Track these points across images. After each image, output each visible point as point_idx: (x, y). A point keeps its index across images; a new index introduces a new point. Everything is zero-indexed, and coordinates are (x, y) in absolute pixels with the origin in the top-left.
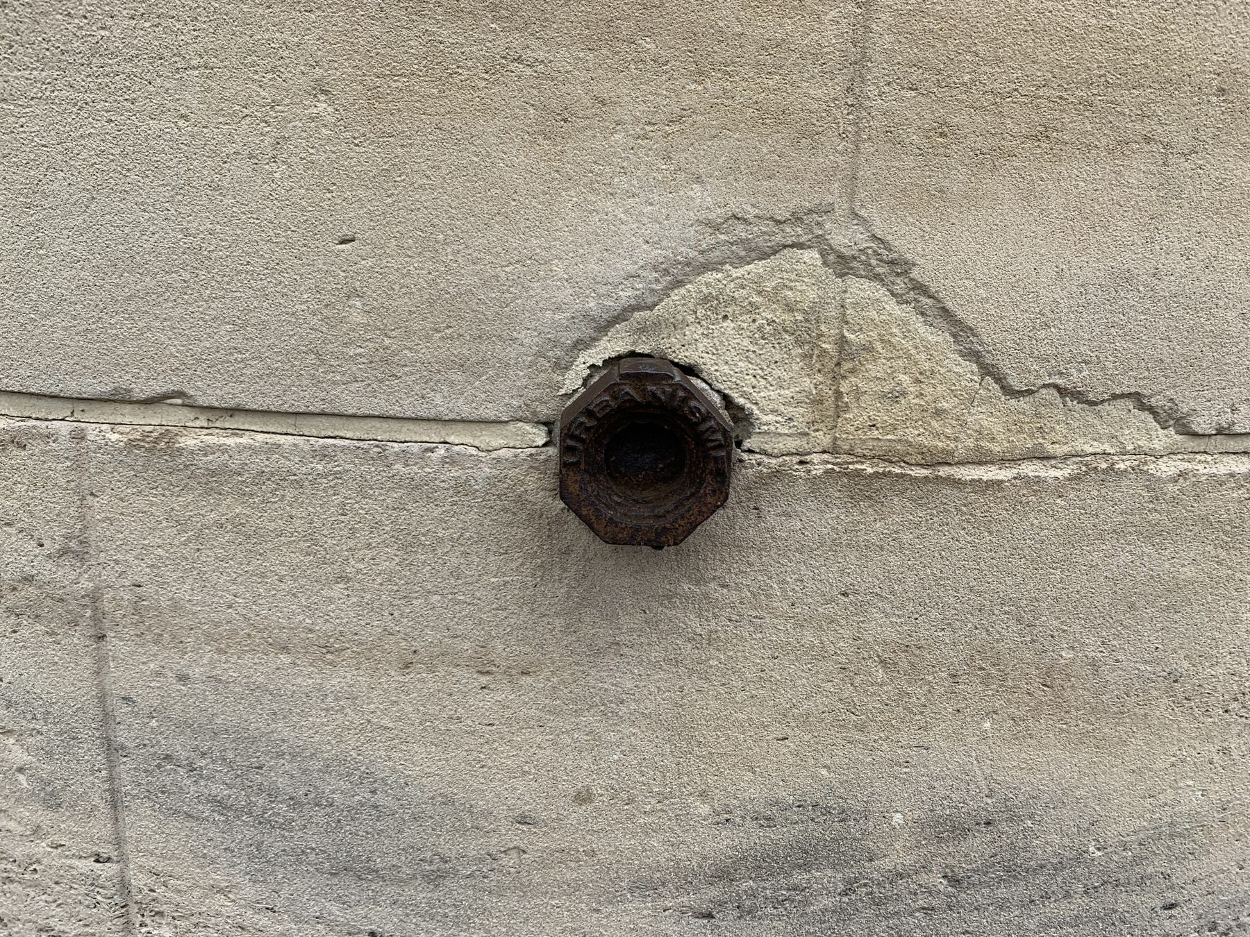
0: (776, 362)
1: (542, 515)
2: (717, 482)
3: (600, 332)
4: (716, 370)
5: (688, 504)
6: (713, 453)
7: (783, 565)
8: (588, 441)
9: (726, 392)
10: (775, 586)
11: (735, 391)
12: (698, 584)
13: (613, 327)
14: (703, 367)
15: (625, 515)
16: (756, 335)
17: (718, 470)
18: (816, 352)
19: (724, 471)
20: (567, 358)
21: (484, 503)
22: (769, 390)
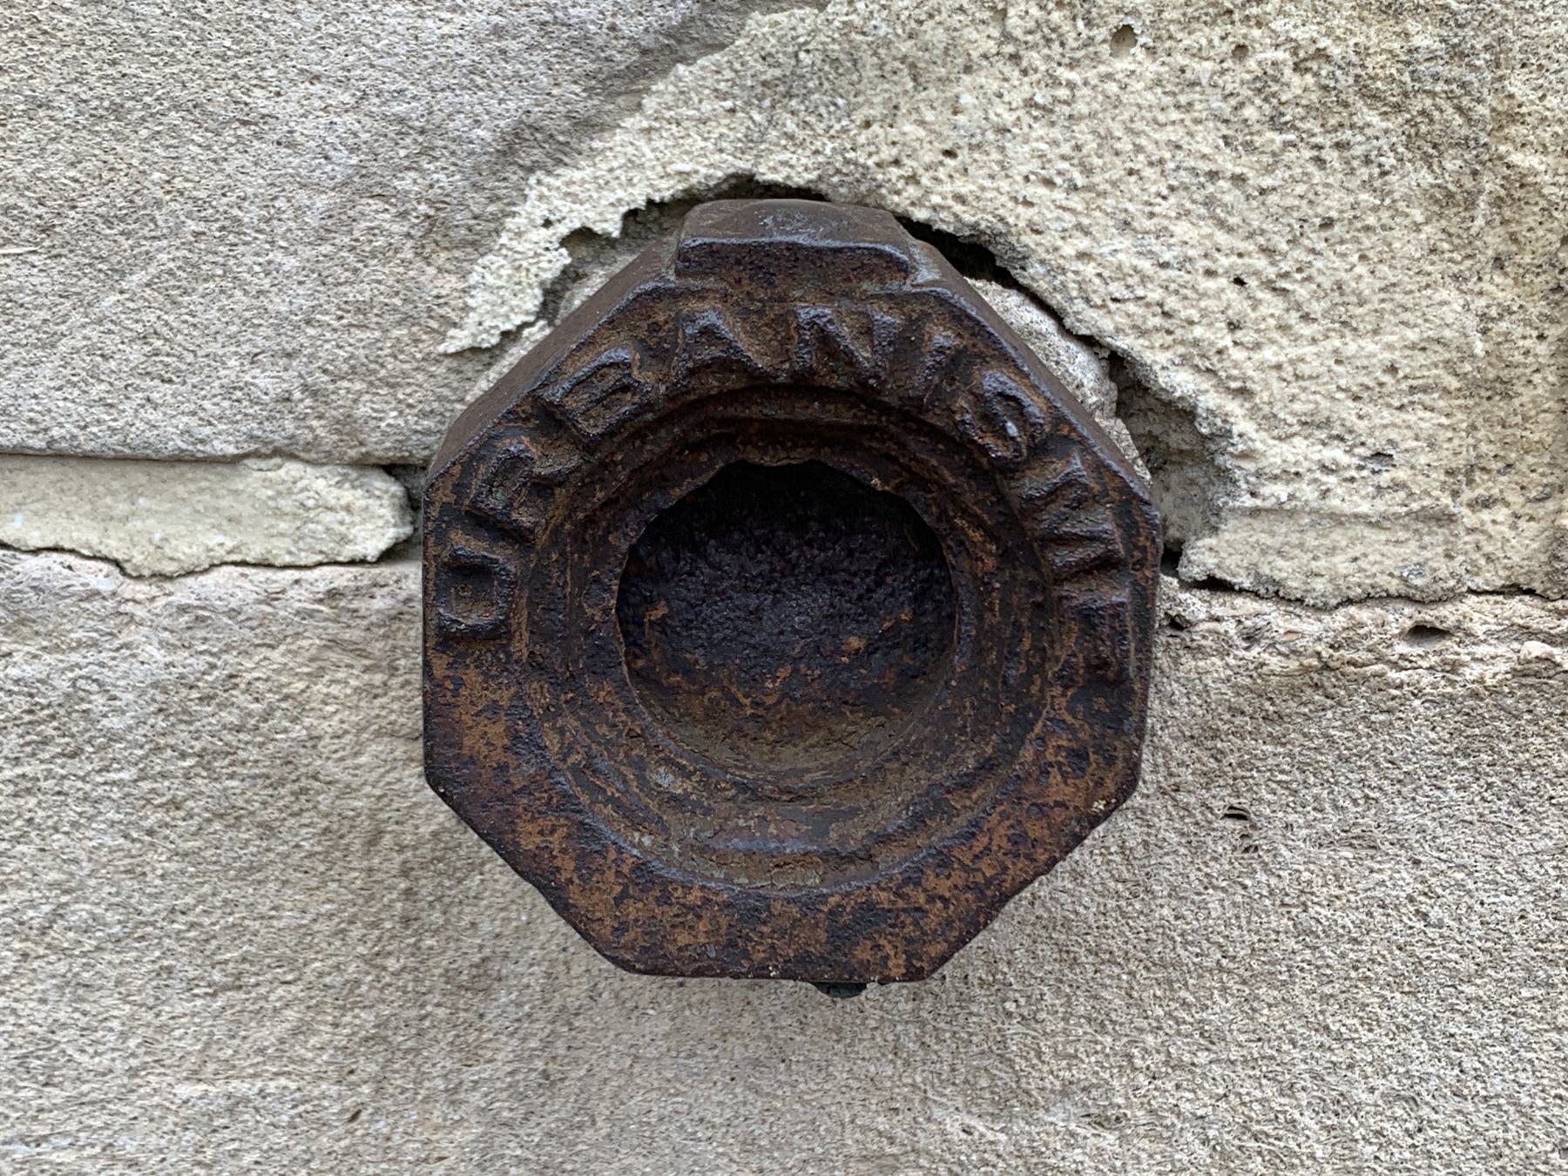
0: (1328, 224)
1: (380, 833)
2: (1092, 715)
3: (612, 96)
4: (1083, 256)
5: (966, 806)
6: (1078, 594)
7: (1339, 1038)
8: (542, 538)
9: (1122, 343)
10: (1307, 1120)
11: (1159, 339)
12: (1001, 1110)
13: (664, 73)
14: (1029, 239)
15: (703, 850)
16: (1249, 112)
17: (1098, 666)
18: (1490, 183)
19: (1123, 670)
20: (477, 202)
21: (146, 785)
22: (1296, 339)
